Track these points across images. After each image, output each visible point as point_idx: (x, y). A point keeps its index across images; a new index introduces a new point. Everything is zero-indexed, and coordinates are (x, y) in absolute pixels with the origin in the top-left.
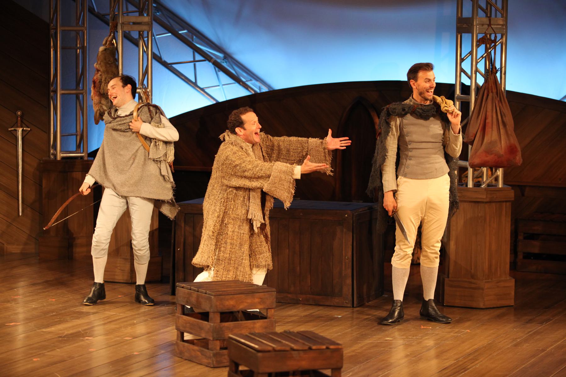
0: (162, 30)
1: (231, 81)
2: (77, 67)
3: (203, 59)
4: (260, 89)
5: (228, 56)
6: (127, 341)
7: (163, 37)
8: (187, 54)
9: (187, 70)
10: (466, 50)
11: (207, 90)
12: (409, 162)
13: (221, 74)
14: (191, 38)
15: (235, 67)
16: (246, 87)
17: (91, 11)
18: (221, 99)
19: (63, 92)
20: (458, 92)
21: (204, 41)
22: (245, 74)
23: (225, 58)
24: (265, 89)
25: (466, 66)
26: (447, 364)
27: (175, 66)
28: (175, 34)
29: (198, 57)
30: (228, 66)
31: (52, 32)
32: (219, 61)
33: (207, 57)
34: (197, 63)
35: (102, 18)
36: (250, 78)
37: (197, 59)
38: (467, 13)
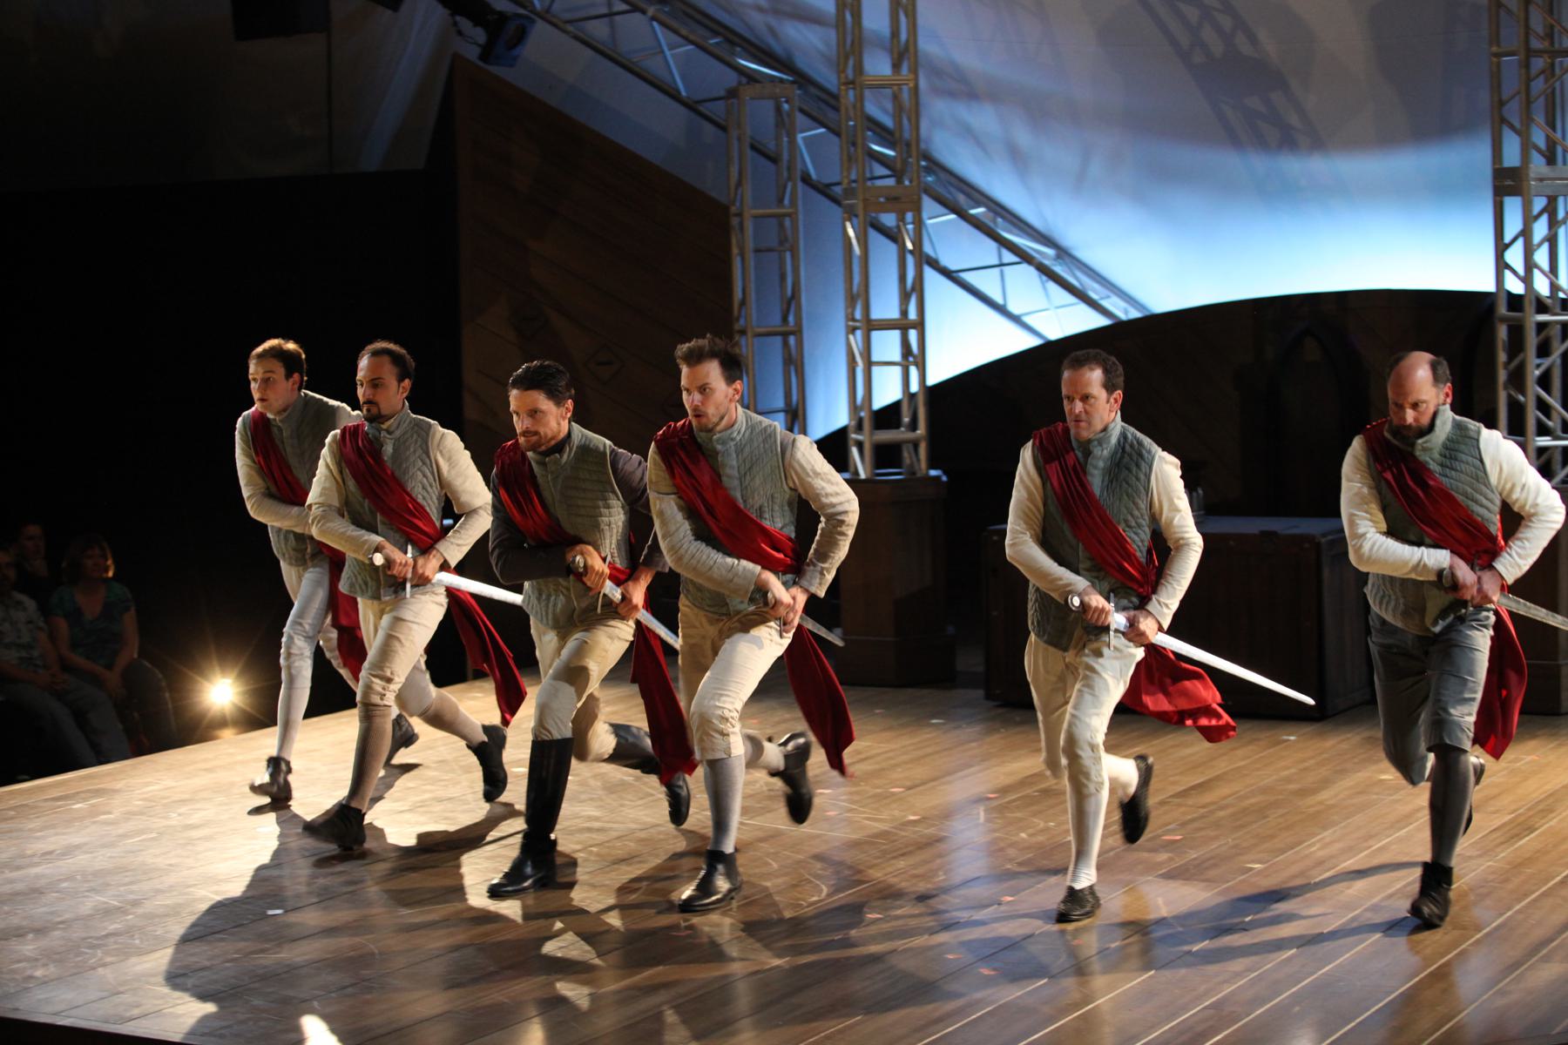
0: (939, 208)
1: (1070, 299)
2: (783, 277)
3: (1016, 259)
4: (1126, 312)
5: (1063, 253)
6: (894, 794)
7: (938, 221)
8: (987, 251)
9: (987, 282)
10: (1513, 226)
11: (1026, 319)
12: (1514, 496)
13: (1052, 286)
14: (992, 221)
15: (1079, 274)
16: (1105, 312)
17: (806, 179)
18: (1054, 334)
19: (811, 625)
20: (1502, 310)
21: (1020, 229)
22: (1096, 286)
23: (1058, 257)
24: (1134, 314)
25: (1515, 256)
26: (1497, 823)
27: (965, 276)
28: (962, 215)
29: (1008, 257)
30: (1060, 269)
31: (735, 221)
32: (1047, 262)
33: (1025, 257)
34: (1006, 269)
35: (824, 190)
36: (1106, 292)
37: (1005, 261)
38: (1512, 158)
